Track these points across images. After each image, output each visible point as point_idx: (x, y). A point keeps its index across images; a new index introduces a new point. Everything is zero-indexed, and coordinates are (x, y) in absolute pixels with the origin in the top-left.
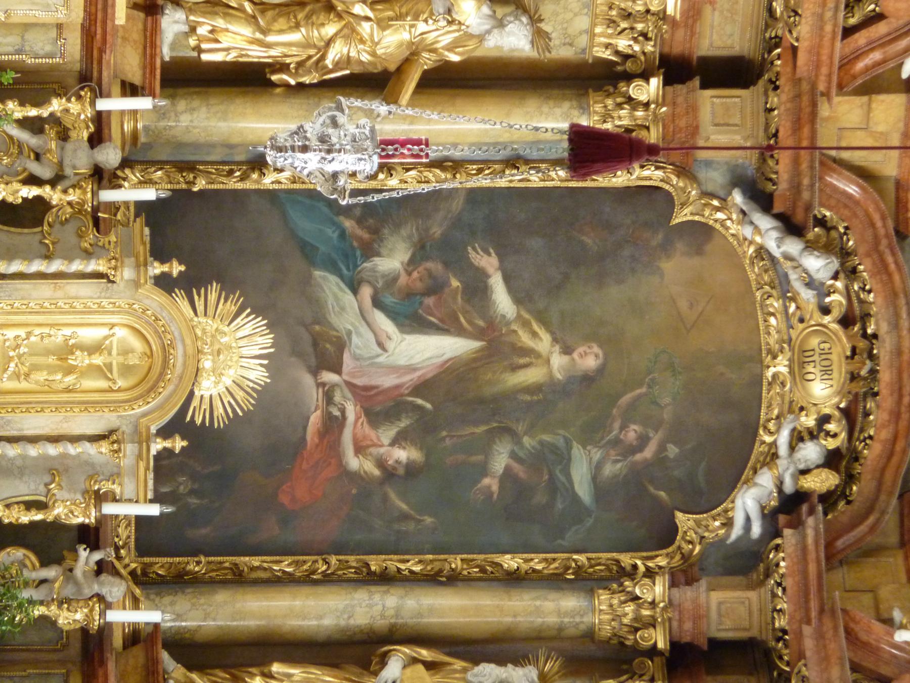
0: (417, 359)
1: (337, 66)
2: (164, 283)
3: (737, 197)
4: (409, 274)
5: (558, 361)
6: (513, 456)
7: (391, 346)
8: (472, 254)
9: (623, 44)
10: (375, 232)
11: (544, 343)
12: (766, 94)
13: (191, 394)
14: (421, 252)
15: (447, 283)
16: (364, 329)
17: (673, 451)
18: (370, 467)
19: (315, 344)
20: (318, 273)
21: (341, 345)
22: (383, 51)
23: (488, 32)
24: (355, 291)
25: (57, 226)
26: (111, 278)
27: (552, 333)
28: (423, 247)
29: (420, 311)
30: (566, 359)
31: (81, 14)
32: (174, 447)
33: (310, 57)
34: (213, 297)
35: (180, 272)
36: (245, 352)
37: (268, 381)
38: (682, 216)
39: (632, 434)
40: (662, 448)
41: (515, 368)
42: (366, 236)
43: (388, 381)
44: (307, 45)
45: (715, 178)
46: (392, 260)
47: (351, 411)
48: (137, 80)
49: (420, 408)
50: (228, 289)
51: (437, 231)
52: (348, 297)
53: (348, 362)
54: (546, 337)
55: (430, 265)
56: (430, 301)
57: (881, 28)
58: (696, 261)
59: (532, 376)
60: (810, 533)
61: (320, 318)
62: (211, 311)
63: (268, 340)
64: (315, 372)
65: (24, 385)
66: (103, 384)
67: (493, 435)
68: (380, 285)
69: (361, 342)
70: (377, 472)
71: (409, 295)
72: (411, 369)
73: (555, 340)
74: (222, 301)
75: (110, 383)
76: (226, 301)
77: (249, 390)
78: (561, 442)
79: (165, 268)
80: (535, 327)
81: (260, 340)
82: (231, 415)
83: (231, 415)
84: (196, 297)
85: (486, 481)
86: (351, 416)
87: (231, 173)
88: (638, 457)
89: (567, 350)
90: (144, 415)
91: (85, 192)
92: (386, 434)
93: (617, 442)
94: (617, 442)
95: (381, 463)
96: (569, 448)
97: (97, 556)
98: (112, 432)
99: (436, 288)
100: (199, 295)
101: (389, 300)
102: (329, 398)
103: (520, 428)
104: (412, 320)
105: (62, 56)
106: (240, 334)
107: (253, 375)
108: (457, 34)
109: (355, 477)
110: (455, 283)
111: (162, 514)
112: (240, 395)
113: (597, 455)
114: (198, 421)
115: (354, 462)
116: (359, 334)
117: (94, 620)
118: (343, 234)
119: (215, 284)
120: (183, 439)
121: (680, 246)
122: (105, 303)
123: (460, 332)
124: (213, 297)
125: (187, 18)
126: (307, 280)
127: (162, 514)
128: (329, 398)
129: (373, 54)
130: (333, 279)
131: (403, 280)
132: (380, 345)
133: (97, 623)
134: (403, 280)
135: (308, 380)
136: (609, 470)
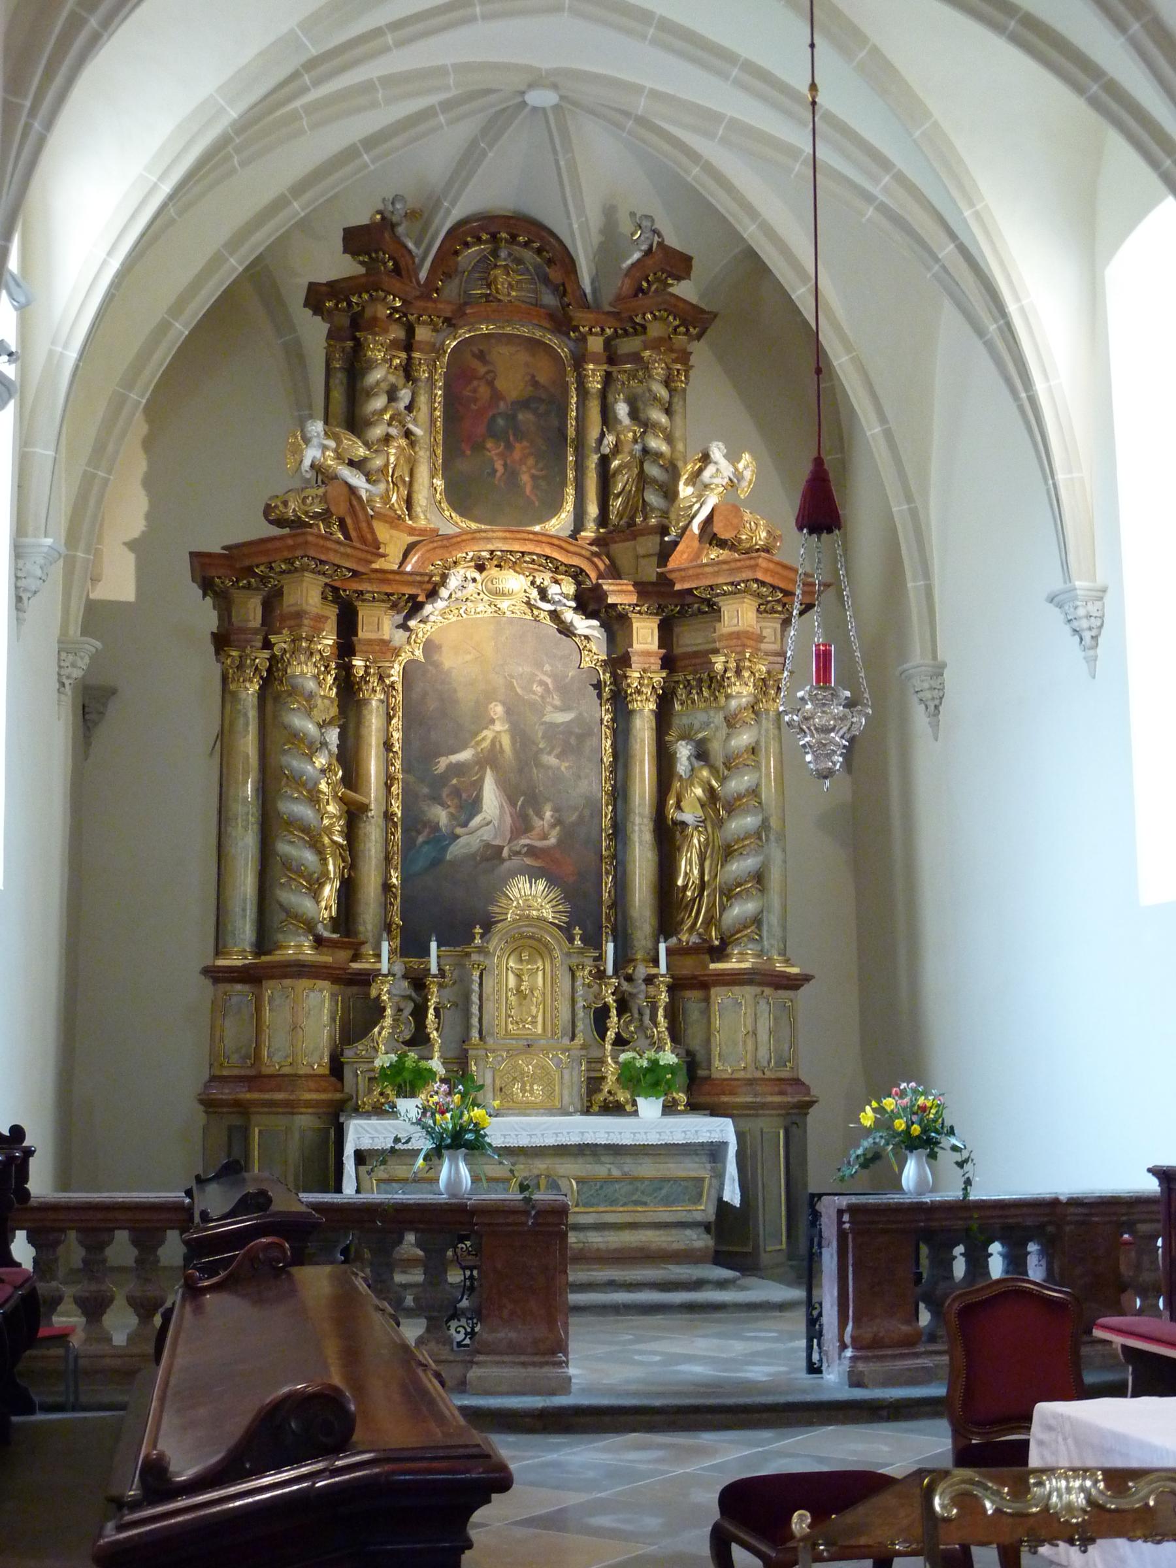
0: (496, 803)
3: (412, 623)
4: (449, 806)
5: (498, 727)
6: (549, 753)
7: (489, 818)
8: (439, 771)
9: (330, 680)
10: (426, 824)
11: (488, 734)
12: (364, 600)
14: (436, 799)
15: (454, 786)
16: (479, 833)
17: (547, 667)
18: (555, 832)
19: (487, 860)
20: (448, 857)
21: (488, 846)
23: (329, 751)
24: (458, 837)
27: (484, 729)
28: (434, 799)
30: (497, 722)
38: (419, 654)
39: (538, 689)
40: (545, 673)
41: (502, 751)
42: (427, 831)
43: (508, 820)
45: (400, 636)
46: (441, 816)
47: (524, 841)
48: (350, 953)
49: (522, 805)
50: (493, 901)
51: (426, 790)
52: (462, 841)
53: (497, 842)
54: (485, 733)
55: (444, 795)
56: (464, 796)
57: (349, 521)
58: (445, 649)
59: (506, 741)
60: (612, 588)
61: (473, 856)
62: (504, 911)
64: (503, 861)
65: (540, 1019)
66: (540, 973)
67: (539, 765)
68: (454, 823)
69: (487, 834)
70: (558, 828)
71: (460, 807)
72: (502, 807)
73: (486, 728)
78: (543, 727)
80: (479, 738)
85: (563, 768)
86: (527, 841)
87: (391, 904)
88: (550, 686)
89: (492, 721)
90: (561, 950)
92: (537, 823)
93: (542, 697)
94: (542, 697)
95: (553, 826)
96: (546, 723)
98: (570, 969)
99: (456, 792)
101: (463, 818)
102: (518, 853)
103: (535, 749)
104: (473, 806)
107: (541, 887)
109: (560, 842)
110: (454, 781)
112: (552, 895)
113: (549, 708)
115: (552, 841)
116: (482, 835)
118: (425, 843)
121: (436, 657)
123: (481, 780)
124: (497, 910)
126: (452, 863)
128: (518, 853)
130: (451, 848)
131: (452, 810)
132: (488, 824)
134: (452, 810)
135: (507, 864)
136: (557, 702)
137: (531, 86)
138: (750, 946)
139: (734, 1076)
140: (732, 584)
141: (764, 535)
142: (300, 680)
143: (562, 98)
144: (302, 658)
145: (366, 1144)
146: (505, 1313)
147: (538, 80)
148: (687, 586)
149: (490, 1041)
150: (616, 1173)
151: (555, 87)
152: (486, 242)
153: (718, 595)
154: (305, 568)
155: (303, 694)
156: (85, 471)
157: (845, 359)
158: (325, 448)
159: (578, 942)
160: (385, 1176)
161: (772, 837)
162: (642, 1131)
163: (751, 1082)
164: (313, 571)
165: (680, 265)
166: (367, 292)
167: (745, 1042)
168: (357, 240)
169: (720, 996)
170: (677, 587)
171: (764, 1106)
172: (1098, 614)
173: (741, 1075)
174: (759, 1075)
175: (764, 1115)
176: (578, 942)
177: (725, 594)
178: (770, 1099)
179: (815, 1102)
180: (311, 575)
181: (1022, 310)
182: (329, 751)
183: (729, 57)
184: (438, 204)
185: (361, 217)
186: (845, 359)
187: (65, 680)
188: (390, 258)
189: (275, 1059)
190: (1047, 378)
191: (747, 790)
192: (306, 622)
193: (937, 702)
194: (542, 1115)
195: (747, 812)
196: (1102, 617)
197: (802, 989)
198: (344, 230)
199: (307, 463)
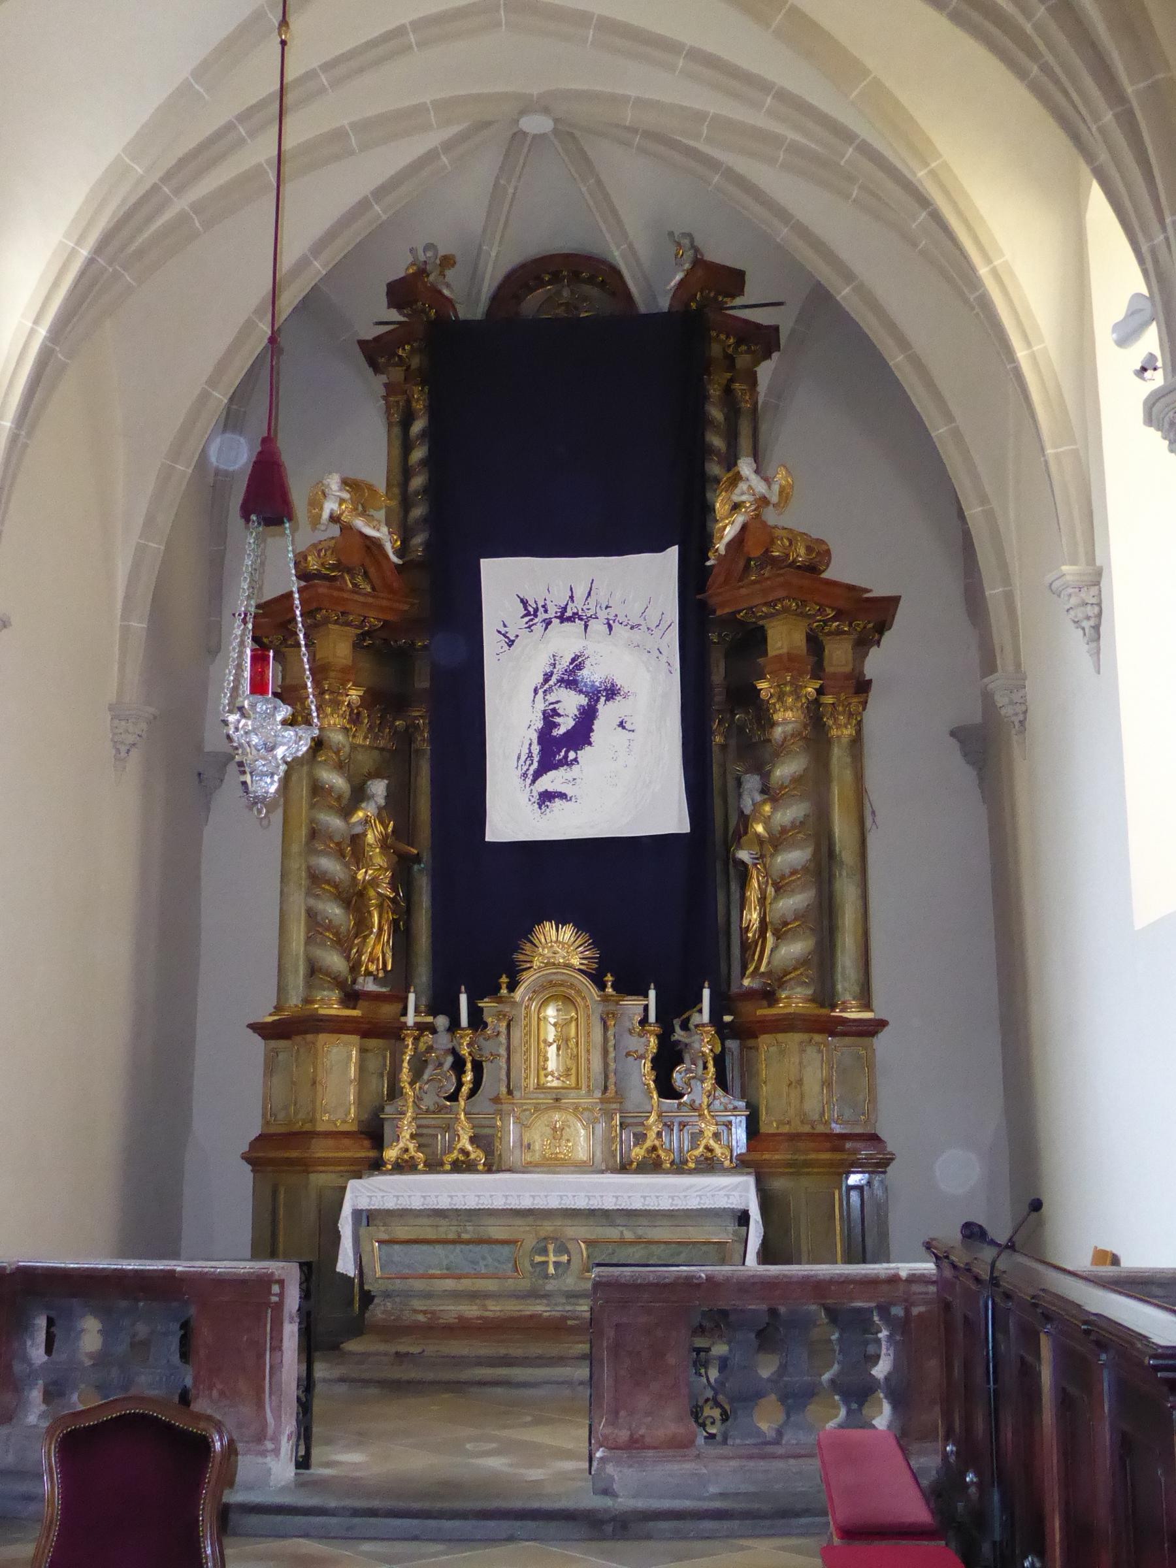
98: (602, 1019)
124: (522, 957)
137: (523, 112)
138: (799, 989)
139: (780, 1131)
141: (802, 551)
143: (556, 121)
144: (329, 710)
145: (364, 1204)
146: (215, 1393)
147: (529, 106)
149: (516, 1094)
150: (629, 1235)
151: (546, 110)
153: (761, 618)
155: (331, 748)
156: (138, 543)
157: (900, 358)
158: (342, 501)
159: (609, 990)
160: (385, 1237)
161: (844, 874)
162: (569, 1194)
163: (794, 1137)
164: (336, 622)
165: (733, 280)
166: (408, 344)
167: (788, 1095)
169: (766, 1043)
170: (719, 613)
171: (807, 1164)
172: (1094, 601)
173: (785, 1129)
174: (807, 1129)
175: (808, 1174)
176: (609, 990)
178: (813, 1156)
179: (892, 1159)
180: (336, 627)
181: (995, 273)
182: (376, 803)
183: (671, 47)
185: (399, 269)
186: (900, 358)
187: (119, 746)
189: (300, 1116)
190: (1029, 344)
193: (1021, 717)
194: (573, 1173)
195: (794, 845)
196: (1099, 605)
197: (880, 1035)
199: (326, 515)
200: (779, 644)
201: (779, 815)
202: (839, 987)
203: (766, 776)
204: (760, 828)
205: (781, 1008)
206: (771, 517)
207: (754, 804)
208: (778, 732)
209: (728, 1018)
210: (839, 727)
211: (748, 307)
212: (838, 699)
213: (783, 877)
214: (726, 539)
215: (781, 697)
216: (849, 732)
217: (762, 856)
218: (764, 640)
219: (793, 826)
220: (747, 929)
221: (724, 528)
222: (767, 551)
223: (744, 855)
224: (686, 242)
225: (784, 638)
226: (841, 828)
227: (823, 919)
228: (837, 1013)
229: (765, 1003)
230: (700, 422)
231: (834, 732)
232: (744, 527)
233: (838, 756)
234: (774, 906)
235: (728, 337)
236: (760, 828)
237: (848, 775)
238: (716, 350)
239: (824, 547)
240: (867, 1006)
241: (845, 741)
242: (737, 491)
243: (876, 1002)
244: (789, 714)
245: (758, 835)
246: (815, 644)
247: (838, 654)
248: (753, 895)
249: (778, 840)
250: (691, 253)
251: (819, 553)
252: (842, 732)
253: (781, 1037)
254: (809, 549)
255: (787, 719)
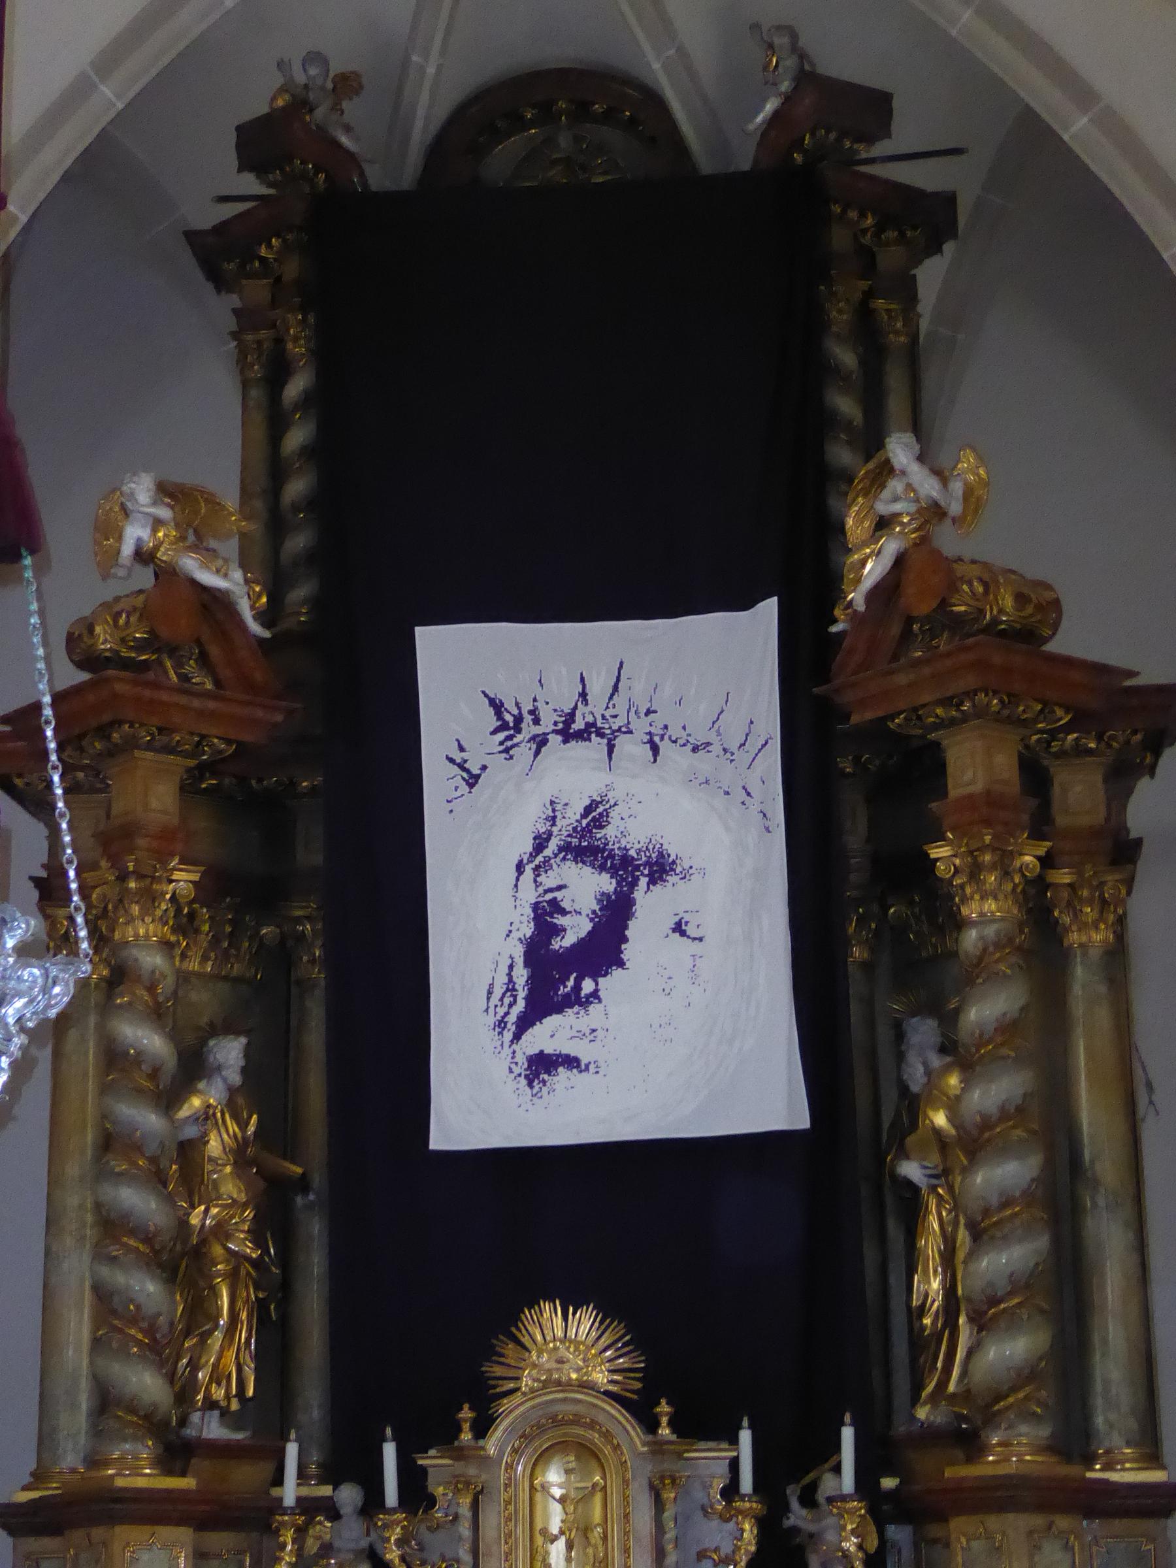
1: (259, 1242)
2: (482, 1428)
13: (607, 1393)
22: (243, 1195)
25: (425, 1555)
26: (479, 1489)
29: (965, 1162)
31: (182, 1529)
32: (667, 1414)
33: (248, 1274)
34: (498, 1371)
35: (470, 1409)
36: (559, 1333)
37: (591, 1306)
44: (233, 1277)
50: (491, 1354)
62: (511, 1373)
63: (547, 1307)
74: (502, 1360)
75: (598, 1488)
76: (503, 1356)
77: (603, 1327)
79: (466, 1426)
81: (546, 1315)
82: (631, 1347)
83: (631, 1347)
84: (498, 1390)
91: (283, 1523)
97: (795, 1504)
100: (494, 1387)
105: (242, 1552)
106: (539, 1337)
108: (227, 1116)
111: (750, 1428)
114: (638, 1385)
117: (751, 1508)
119: (483, 1369)
120: (659, 1403)
122: (504, 1496)
124: (498, 1371)
125: (199, 1410)
127: (854, 1423)
129: (245, 1206)
133: (754, 1505)
138: (1023, 1428)
140: (946, 702)
141: (1008, 602)
142: (135, 952)
144: (136, 909)
148: (869, 715)
152: (532, 123)
153: (936, 727)
154: (131, 744)
155: (138, 979)
158: (157, 523)
159: (665, 1431)
161: (1101, 1202)
164: (149, 747)
165: (872, 109)
166: (278, 236)
168: (260, 144)
176: (665, 1431)
177: (941, 724)
180: (150, 755)
184: (406, 63)
188: (317, 169)
191: (1003, 1109)
192: (141, 842)
195: (1005, 1151)
198: (238, 128)
199: (128, 549)
200: (969, 775)
201: (976, 1094)
202: (1099, 1421)
203: (949, 1020)
204: (940, 1119)
205: (991, 1464)
206: (948, 541)
207: (928, 1073)
208: (971, 939)
209: (889, 1483)
210: (1083, 927)
211: (903, 156)
212: (1080, 874)
213: (986, 1212)
214: (867, 584)
215: (975, 872)
216: (1100, 937)
217: (946, 1172)
218: (940, 768)
219: (1004, 1114)
220: (922, 1310)
221: (863, 563)
222: (944, 603)
223: (911, 1170)
224: (781, 41)
225: (976, 764)
226: (1092, 1113)
227: (1065, 1290)
228: (1096, 1473)
229: (959, 1454)
230: (815, 371)
231: (1074, 938)
232: (900, 562)
233: (1083, 980)
234: (972, 1267)
235: (863, 215)
236: (940, 1119)
237: (1103, 1017)
238: (839, 239)
239: (1049, 595)
240: (1153, 1457)
241: (1095, 954)
242: (886, 494)
243: (1167, 1459)
244: (990, 906)
245: (937, 1132)
246: (1035, 776)
247: (1078, 792)
248: (930, 1245)
249: (973, 1142)
250: (790, 62)
251: (1040, 607)
252: (1088, 937)
253: (993, 1522)
254: (1021, 599)
255: (986, 913)
